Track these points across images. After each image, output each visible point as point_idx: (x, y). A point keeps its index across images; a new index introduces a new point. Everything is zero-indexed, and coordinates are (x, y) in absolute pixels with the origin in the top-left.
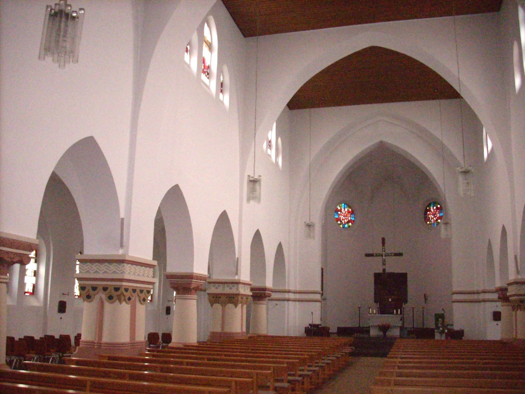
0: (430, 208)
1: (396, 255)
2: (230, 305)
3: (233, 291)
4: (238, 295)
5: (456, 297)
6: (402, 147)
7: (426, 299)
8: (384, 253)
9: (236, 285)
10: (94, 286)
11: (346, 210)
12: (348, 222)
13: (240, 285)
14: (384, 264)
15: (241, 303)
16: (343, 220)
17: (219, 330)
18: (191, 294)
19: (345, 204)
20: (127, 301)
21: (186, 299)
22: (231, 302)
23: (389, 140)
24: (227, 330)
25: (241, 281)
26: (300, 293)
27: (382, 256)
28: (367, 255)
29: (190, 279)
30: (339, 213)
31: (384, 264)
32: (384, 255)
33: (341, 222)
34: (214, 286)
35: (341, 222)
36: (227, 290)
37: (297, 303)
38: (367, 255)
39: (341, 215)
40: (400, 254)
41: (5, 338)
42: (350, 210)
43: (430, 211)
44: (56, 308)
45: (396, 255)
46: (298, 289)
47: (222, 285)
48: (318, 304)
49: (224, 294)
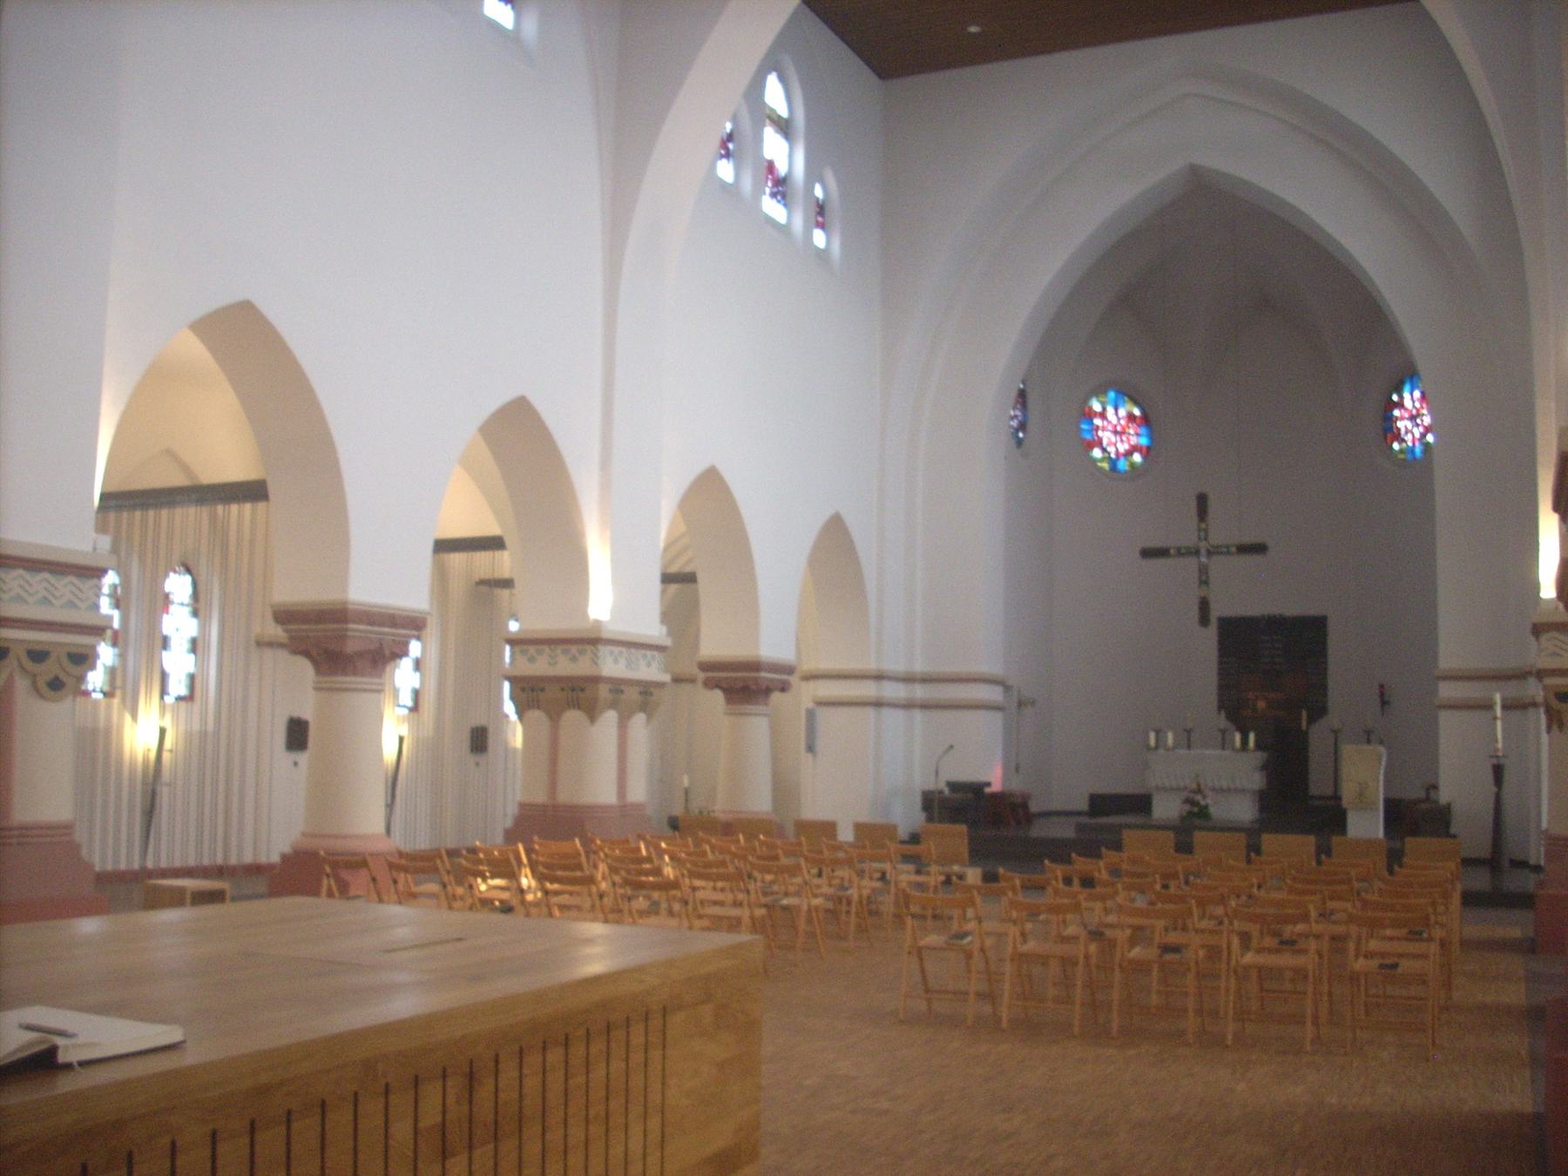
0: (1401, 398)
1: (1244, 549)
2: (572, 717)
3: (581, 668)
4: (596, 680)
5: (1447, 691)
6: (1245, 174)
7: (1384, 703)
8: (1203, 544)
9: (589, 648)
10: (38, 648)
11: (1122, 412)
12: (1129, 453)
13: (604, 650)
14: (1204, 582)
15: (613, 705)
16: (1110, 444)
17: (540, 797)
18: (346, 675)
19: (1120, 392)
20: (45, 689)
21: (338, 690)
22: (576, 704)
23: (1214, 161)
24: (563, 797)
25: (605, 635)
26: (926, 680)
27: (1197, 553)
28: (1147, 553)
29: (338, 621)
30: (1097, 421)
31: (1204, 582)
32: (1203, 551)
33: (1104, 450)
34: (565, 652)
35: (1104, 450)
36: (565, 666)
37: (918, 715)
38: (1147, 553)
39: (1104, 429)
40: (1259, 549)
41: (851, 827)
42: (1137, 412)
43: (1400, 405)
44: (466, 744)
45: (1244, 549)
46: (919, 667)
47: (546, 649)
48: (997, 718)
49: (557, 680)
